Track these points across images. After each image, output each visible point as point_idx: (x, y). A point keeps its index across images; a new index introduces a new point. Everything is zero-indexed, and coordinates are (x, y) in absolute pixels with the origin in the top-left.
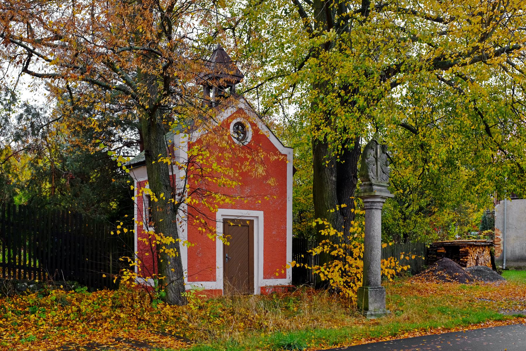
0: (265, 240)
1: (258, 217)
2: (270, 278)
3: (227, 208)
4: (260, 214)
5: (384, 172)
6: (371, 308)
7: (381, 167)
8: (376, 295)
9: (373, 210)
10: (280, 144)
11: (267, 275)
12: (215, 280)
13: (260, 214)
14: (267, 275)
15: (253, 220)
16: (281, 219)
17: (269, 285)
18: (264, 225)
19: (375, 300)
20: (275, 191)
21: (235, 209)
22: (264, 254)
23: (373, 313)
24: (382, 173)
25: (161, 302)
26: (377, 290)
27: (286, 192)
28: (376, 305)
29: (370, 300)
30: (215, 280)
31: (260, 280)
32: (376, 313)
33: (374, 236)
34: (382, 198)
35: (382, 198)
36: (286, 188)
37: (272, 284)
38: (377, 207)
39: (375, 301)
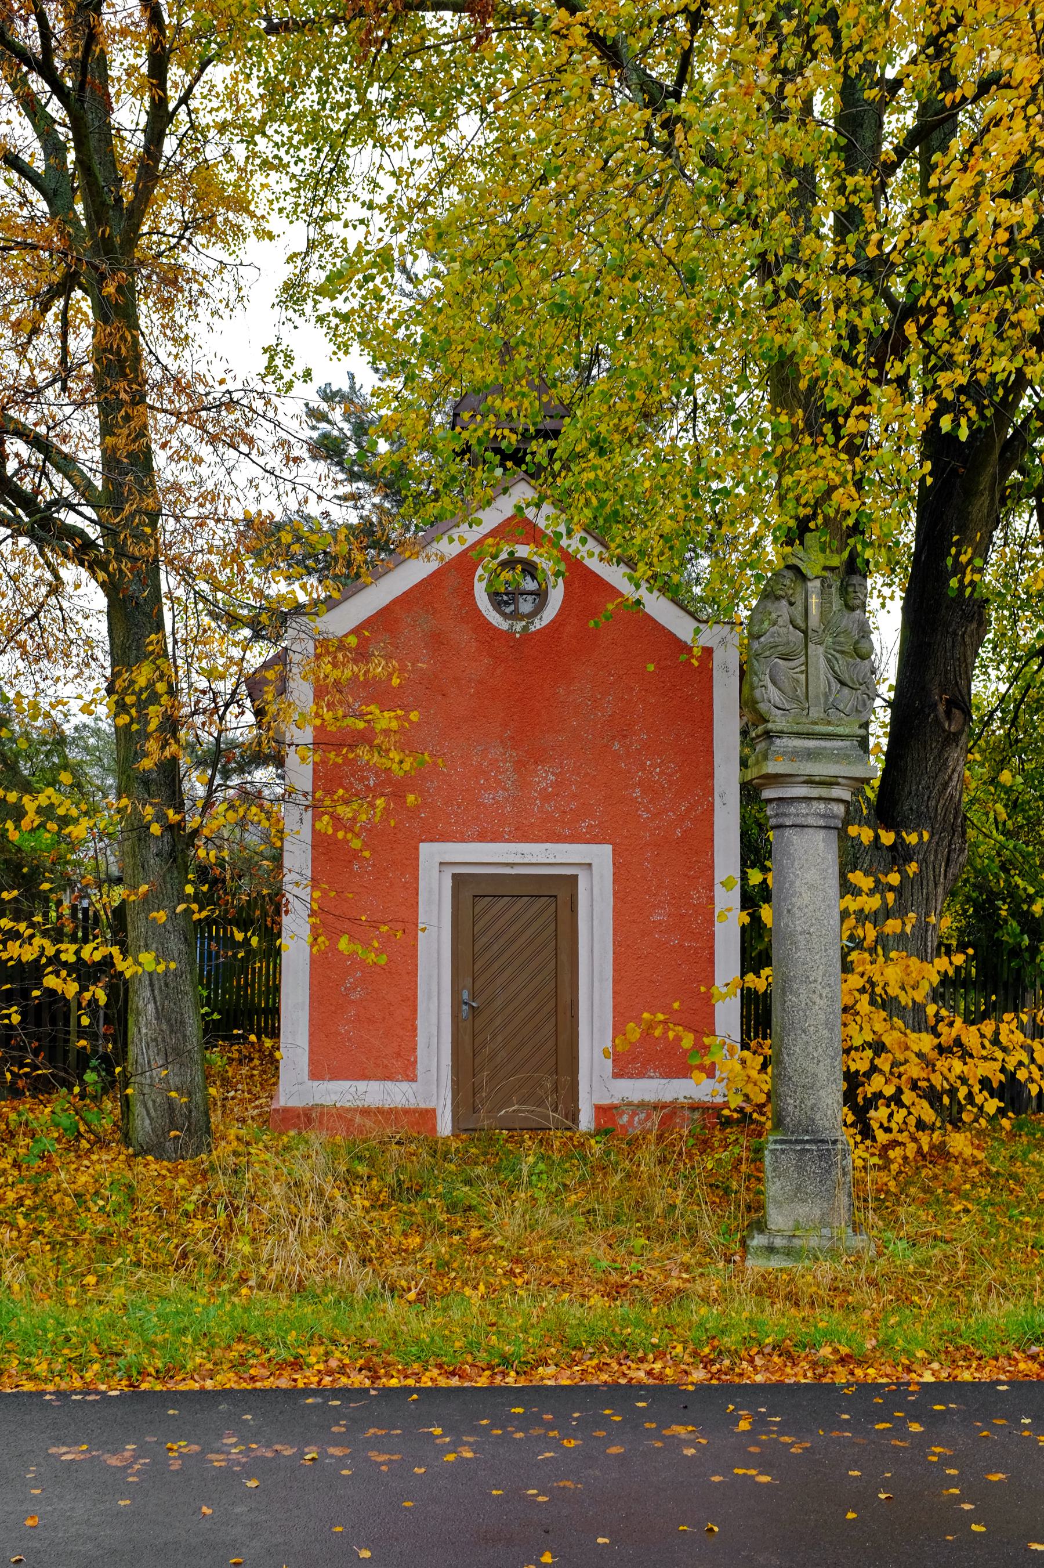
0: (617, 944)
1: (593, 866)
2: (641, 1075)
3: (463, 841)
4: (432, 855)
5: (843, 683)
6: (777, 1219)
7: (829, 661)
8: (800, 1169)
9: (787, 832)
10: (682, 613)
11: (626, 1063)
12: (316, 1074)
14: (626, 1063)
16: (690, 869)
19: (798, 1189)
20: (662, 773)
21: (492, 841)
22: (615, 993)
23: (779, 1242)
24: (835, 686)
27: (711, 776)
28: (807, 1211)
29: (774, 1188)
30: (316, 1074)
31: (597, 1083)
32: (796, 1242)
33: (792, 935)
34: (810, 781)
35: (810, 781)
36: (711, 763)
37: (651, 1097)
38: (799, 821)
39: (798, 1194)
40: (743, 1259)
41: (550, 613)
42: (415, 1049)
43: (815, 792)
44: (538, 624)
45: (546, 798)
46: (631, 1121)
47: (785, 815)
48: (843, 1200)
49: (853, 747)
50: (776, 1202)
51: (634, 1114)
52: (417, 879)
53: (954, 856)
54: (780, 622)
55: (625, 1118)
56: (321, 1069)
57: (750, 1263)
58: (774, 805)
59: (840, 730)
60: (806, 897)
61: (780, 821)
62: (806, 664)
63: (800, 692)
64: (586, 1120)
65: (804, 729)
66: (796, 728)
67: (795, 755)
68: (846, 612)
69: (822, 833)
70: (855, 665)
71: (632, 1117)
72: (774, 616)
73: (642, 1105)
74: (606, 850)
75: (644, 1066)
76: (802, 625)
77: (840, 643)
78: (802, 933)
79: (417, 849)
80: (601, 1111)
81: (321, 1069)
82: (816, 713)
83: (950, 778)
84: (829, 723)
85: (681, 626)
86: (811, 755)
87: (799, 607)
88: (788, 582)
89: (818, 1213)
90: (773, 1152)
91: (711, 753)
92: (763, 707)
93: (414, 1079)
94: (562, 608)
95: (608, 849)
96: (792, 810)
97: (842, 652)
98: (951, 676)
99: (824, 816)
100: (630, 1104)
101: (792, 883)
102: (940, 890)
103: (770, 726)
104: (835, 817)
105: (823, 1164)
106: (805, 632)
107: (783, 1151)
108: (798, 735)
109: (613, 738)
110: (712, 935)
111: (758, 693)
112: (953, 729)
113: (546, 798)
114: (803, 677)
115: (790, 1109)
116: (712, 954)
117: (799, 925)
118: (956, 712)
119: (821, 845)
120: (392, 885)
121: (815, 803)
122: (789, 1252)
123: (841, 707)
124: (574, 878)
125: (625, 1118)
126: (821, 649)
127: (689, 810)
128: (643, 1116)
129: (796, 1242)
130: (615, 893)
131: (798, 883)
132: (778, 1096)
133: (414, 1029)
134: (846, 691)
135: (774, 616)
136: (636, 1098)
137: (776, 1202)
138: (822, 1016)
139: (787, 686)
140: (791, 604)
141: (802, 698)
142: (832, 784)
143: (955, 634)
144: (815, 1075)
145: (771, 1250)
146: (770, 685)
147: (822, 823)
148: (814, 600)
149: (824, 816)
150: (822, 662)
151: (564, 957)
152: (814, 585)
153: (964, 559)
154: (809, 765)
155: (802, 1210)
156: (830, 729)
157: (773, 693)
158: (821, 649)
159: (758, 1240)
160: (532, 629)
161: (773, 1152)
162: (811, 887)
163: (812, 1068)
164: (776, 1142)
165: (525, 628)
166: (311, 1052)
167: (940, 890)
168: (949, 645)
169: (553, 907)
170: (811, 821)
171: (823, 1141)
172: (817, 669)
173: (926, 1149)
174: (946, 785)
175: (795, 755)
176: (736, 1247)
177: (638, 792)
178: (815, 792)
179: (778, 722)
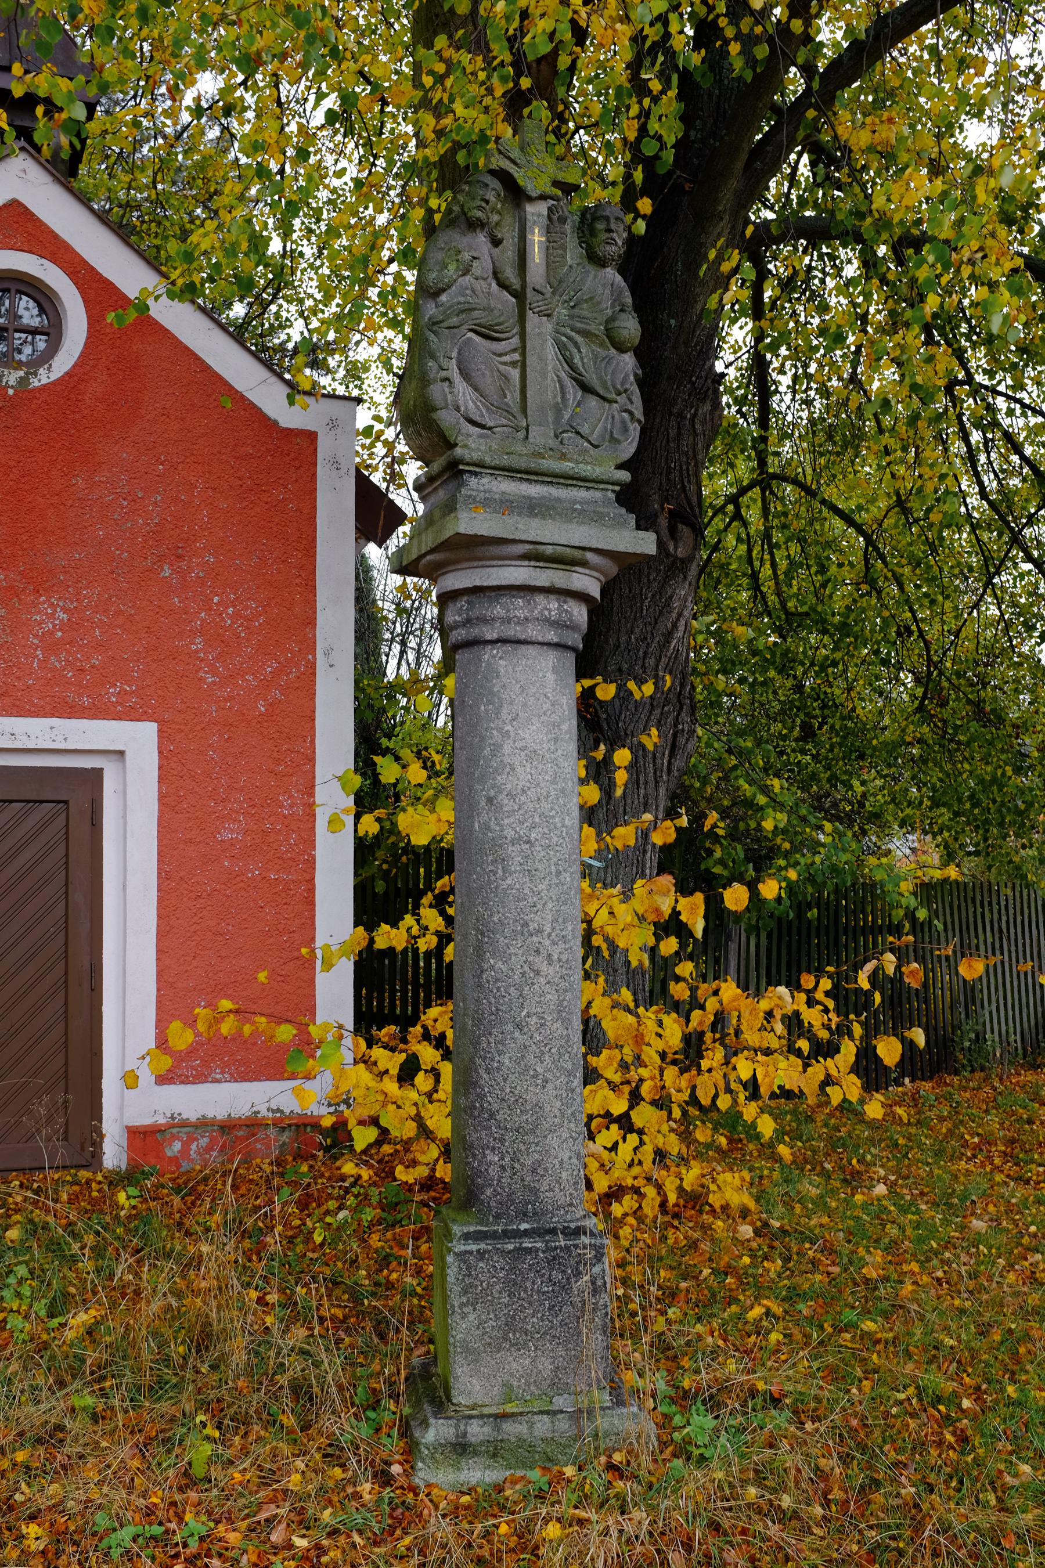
0: (164, 876)
1: (129, 760)
4: (139, 740)
5: (586, 388)
6: (471, 1385)
7: (561, 348)
8: (513, 1286)
9: (488, 654)
13: (139, 740)
15: (98, 773)
16: (278, 762)
17: (192, 1116)
18: (162, 798)
19: (510, 1324)
20: (237, 615)
22: (160, 951)
23: (477, 1431)
24: (574, 393)
25: (615, 1131)
26: (521, 1251)
27: (312, 622)
29: (465, 1326)
31: (134, 1094)
39: (511, 1333)
40: (410, 1470)
41: (64, 362)
43: (543, 577)
44: (44, 377)
45: (51, 646)
46: (185, 1150)
47: (484, 620)
48: (595, 1341)
49: (606, 502)
50: (468, 1351)
51: (191, 1139)
53: (681, 741)
54: (477, 268)
55: (177, 1146)
57: (423, 1475)
58: (462, 602)
59: (586, 470)
60: (523, 774)
61: (475, 632)
62: (523, 350)
63: (512, 398)
64: (113, 1154)
65: (523, 464)
66: (506, 461)
67: (506, 505)
68: (591, 269)
69: (551, 657)
70: (609, 360)
71: (186, 1145)
72: (466, 256)
73: (203, 1124)
74: (148, 731)
75: (205, 1063)
76: (515, 282)
77: (582, 318)
80: (142, 1138)
82: (541, 436)
83: (675, 626)
84: (563, 457)
85: (269, 397)
86: (533, 508)
87: (508, 252)
88: (491, 197)
89: (546, 1366)
90: (461, 1256)
91: (311, 587)
92: (446, 418)
94: (83, 355)
96: (499, 611)
97: (586, 334)
98: (675, 476)
99: (556, 624)
100: (184, 1124)
101: (497, 748)
102: (662, 791)
103: (458, 451)
104: (573, 627)
105: (557, 1276)
106: (519, 296)
107: (481, 1254)
108: (511, 472)
109: (161, 559)
110: (311, 863)
111: (437, 391)
112: (681, 553)
113: (51, 646)
114: (515, 374)
115: (493, 1171)
116: (312, 891)
117: (510, 827)
118: (684, 530)
119: (551, 677)
121: (540, 599)
122: (495, 1451)
123: (585, 430)
124: (97, 774)
125: (177, 1146)
126: (548, 326)
127: (277, 673)
128: (204, 1142)
129: (510, 1428)
131: (507, 749)
132: (468, 1148)
134: (593, 402)
135: (466, 256)
136: (192, 1115)
137: (468, 1351)
139: (489, 383)
140: (496, 242)
141: (516, 409)
142: (574, 563)
143: (681, 416)
144: (538, 1106)
145: (461, 1448)
147: (552, 636)
148: (537, 238)
149: (556, 624)
150: (551, 351)
151: (78, 897)
152: (536, 211)
153: (726, 267)
154: (535, 523)
155: (517, 1364)
156: (567, 466)
157: (462, 390)
158: (548, 326)
159: (436, 1432)
160: (35, 383)
161: (461, 1256)
162: (532, 755)
163: (532, 1094)
164: (466, 1237)
165: (23, 381)
167: (662, 791)
168: (673, 432)
169: (61, 820)
170: (533, 632)
171: (553, 1231)
172: (542, 359)
173: (672, 1198)
174: (669, 636)
175: (506, 505)
176: (392, 1444)
177: (198, 644)
178: (543, 577)
179: (472, 445)
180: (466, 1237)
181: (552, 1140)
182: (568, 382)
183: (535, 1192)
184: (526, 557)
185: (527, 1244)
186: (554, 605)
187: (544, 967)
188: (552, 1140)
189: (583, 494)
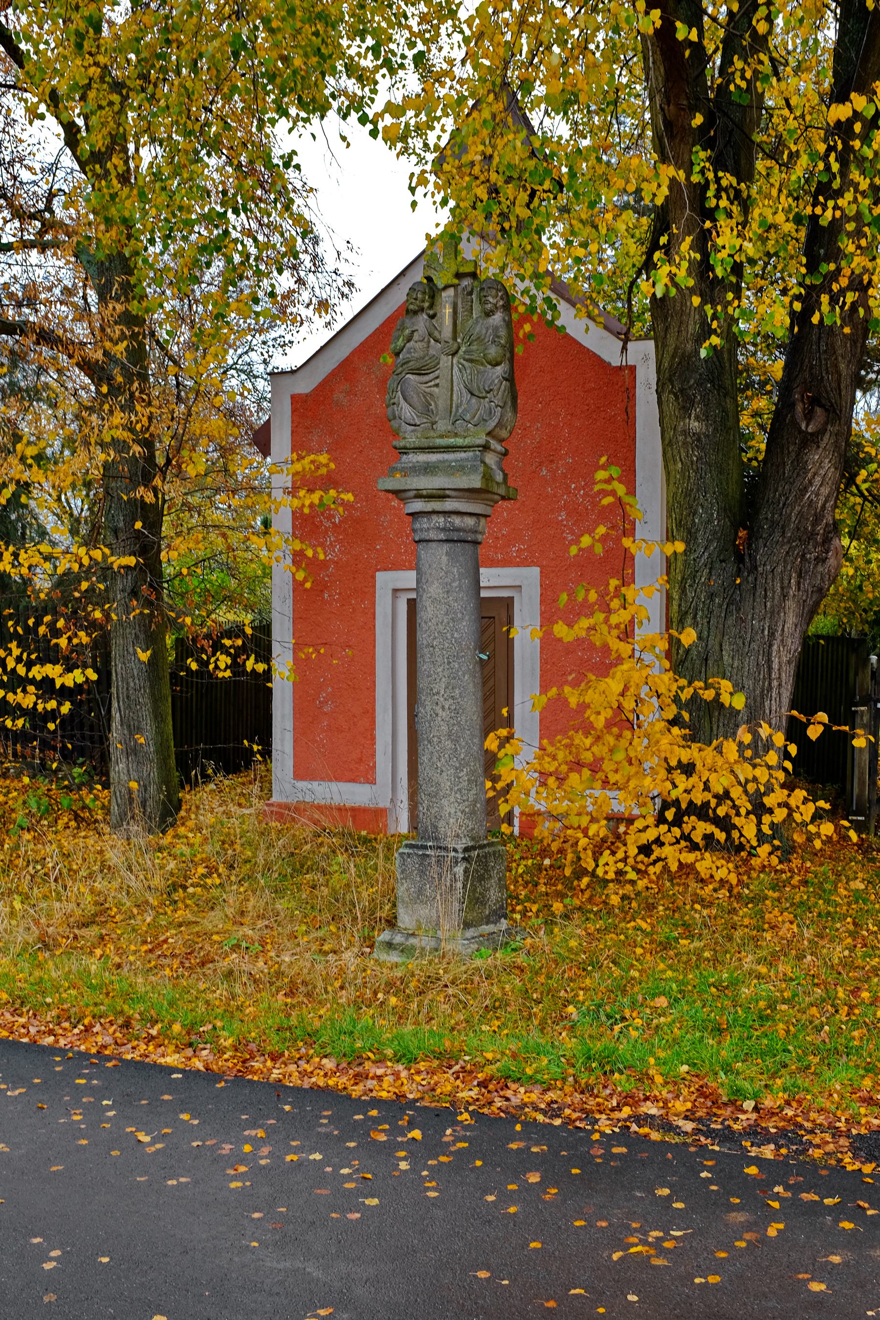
8: (422, 873)
19: (420, 891)
35: (419, 495)
39: (419, 896)
42: (373, 755)
52: (374, 604)
56: (301, 772)
66: (425, 443)
69: (446, 547)
78: (428, 646)
79: (374, 577)
81: (301, 772)
82: (442, 425)
83: (811, 483)
84: (456, 435)
86: (428, 469)
93: (373, 782)
95: (536, 571)
99: (444, 530)
107: (409, 855)
109: (541, 464)
119: (445, 558)
120: (354, 610)
121: (435, 518)
124: (511, 599)
130: (542, 613)
133: (373, 738)
138: (444, 728)
144: (438, 784)
145: (389, 945)
146: (402, 401)
147: (442, 536)
149: (444, 530)
161: (401, 854)
162: (434, 601)
163: (436, 777)
164: (407, 846)
166: (295, 756)
170: (432, 535)
174: (805, 490)
180: (407, 846)
181: (445, 802)
182: (464, 390)
183: (436, 827)
184: (416, 497)
185: (429, 852)
186: (442, 520)
187: (440, 712)
188: (445, 802)
189: (463, 455)
